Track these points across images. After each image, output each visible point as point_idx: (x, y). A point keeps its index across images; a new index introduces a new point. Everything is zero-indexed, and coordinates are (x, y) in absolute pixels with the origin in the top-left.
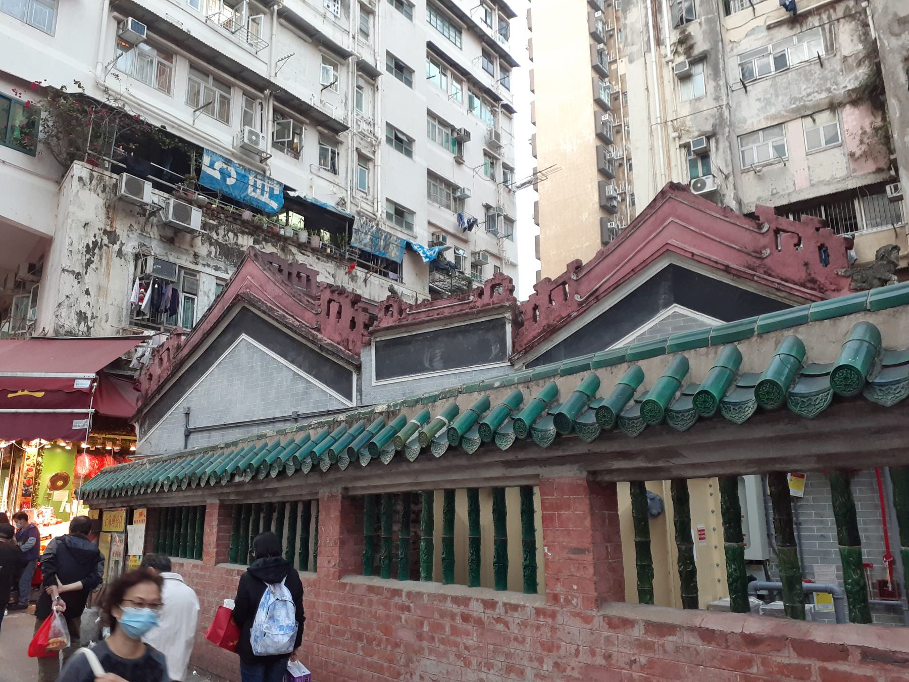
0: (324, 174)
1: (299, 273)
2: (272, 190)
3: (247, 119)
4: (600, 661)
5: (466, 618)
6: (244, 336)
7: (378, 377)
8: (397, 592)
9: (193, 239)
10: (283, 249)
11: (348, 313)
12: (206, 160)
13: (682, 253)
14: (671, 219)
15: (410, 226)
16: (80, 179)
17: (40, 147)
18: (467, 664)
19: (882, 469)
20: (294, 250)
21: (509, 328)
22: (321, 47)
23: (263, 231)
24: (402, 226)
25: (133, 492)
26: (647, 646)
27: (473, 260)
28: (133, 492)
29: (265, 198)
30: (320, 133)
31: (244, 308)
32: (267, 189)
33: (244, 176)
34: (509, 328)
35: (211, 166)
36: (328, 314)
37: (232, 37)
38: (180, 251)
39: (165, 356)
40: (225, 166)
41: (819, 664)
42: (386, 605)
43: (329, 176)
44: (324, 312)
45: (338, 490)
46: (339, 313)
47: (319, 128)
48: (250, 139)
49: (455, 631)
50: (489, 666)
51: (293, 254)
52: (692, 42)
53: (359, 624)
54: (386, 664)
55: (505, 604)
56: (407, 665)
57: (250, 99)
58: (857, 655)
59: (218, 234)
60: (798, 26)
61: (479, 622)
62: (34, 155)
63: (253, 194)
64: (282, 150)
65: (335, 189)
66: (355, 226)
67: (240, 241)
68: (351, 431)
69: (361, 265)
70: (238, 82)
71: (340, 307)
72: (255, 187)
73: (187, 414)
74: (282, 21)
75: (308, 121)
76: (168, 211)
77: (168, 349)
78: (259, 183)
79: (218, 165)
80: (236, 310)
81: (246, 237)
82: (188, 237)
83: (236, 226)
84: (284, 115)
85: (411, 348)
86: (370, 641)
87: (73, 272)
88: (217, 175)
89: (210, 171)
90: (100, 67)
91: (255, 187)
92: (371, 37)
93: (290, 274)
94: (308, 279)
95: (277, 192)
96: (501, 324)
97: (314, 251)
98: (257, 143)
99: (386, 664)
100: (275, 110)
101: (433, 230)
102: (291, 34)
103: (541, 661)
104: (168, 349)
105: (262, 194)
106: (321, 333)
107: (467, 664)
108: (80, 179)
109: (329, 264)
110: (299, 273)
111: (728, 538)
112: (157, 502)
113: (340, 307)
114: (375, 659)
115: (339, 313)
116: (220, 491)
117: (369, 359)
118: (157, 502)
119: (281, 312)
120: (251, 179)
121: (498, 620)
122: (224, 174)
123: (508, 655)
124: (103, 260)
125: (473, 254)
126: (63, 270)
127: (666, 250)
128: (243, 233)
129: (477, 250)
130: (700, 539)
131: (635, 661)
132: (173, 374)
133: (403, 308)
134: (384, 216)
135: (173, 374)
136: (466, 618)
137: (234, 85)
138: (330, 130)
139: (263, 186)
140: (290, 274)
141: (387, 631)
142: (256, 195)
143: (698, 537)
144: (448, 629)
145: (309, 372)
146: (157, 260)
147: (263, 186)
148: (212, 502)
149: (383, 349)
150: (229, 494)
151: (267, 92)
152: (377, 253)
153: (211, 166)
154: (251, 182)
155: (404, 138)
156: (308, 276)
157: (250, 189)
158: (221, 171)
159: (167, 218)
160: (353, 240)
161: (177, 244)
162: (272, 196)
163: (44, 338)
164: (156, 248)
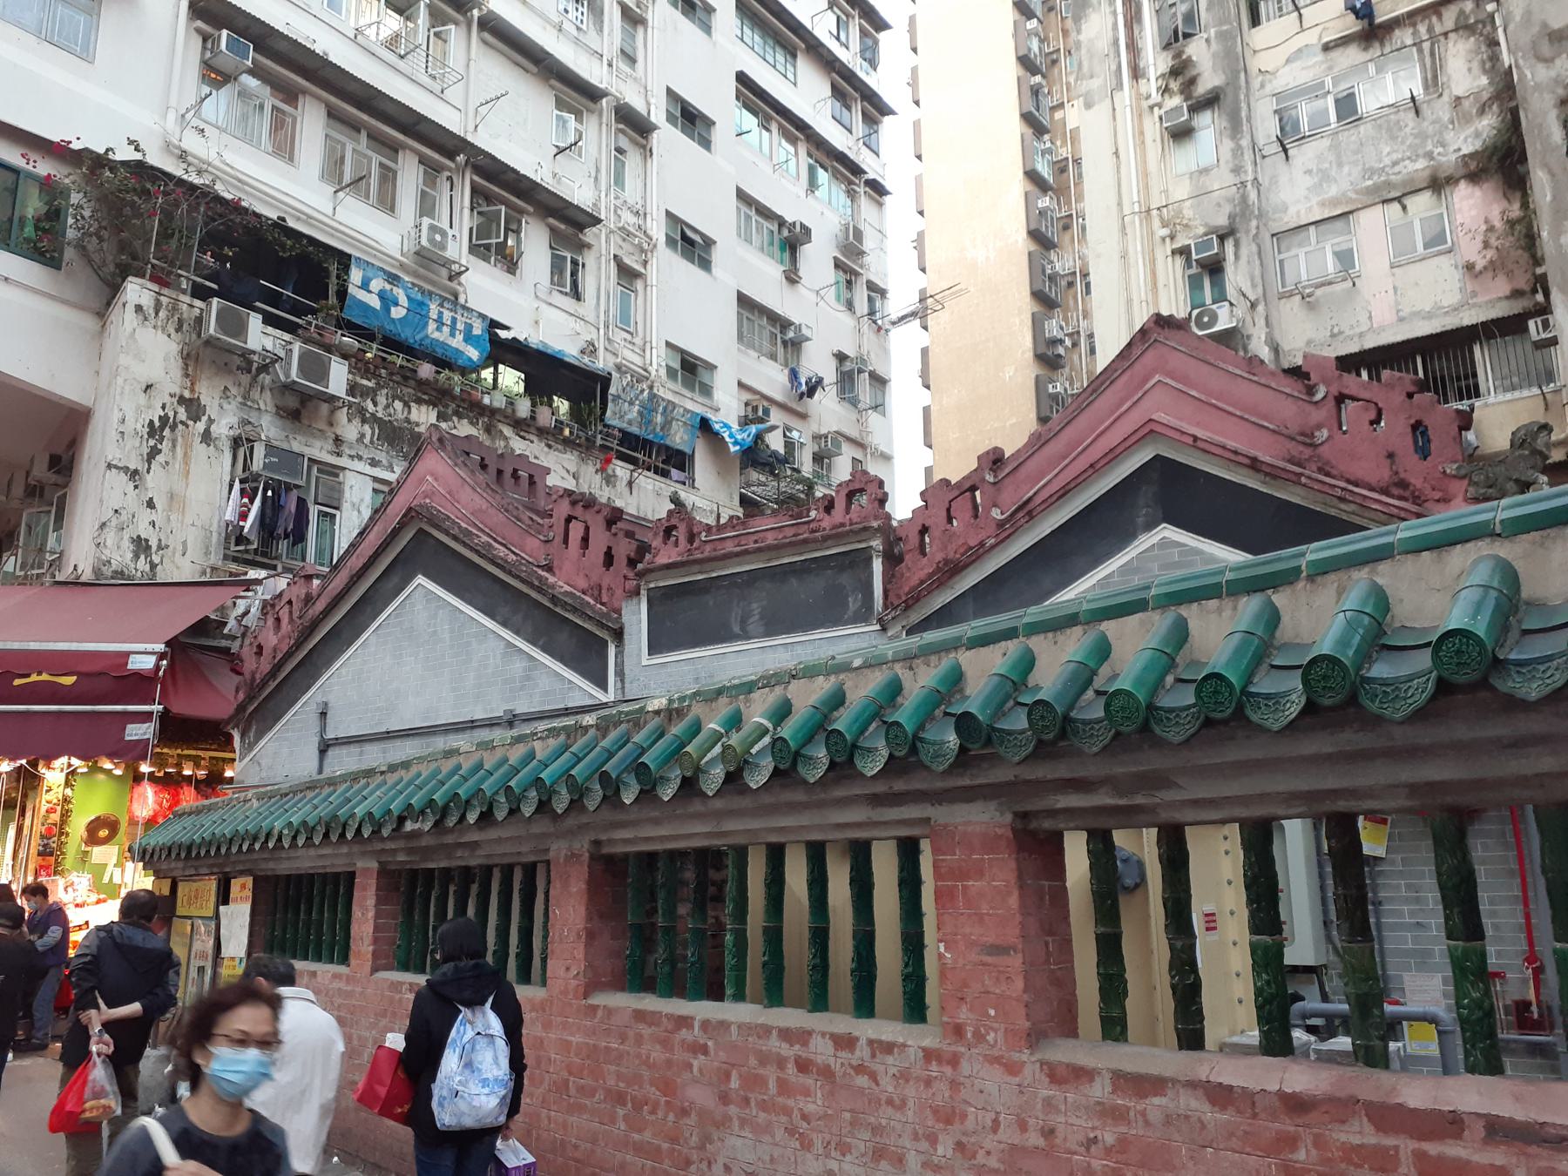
0: (559, 299)
1: (515, 471)
2: (469, 327)
3: (426, 206)
4: (1034, 1139)
5: (803, 1066)
6: (420, 580)
7: (653, 650)
8: (684, 1022)
9: (333, 412)
10: (488, 430)
11: (600, 540)
12: (356, 276)
13: (1177, 436)
14: (1157, 378)
15: (706, 391)
16: (139, 308)
17: (69, 253)
18: (806, 1145)
19: (1522, 808)
20: (507, 431)
21: (877, 566)
22: (553, 82)
23: (454, 398)
24: (693, 390)
25: (229, 849)
26: (1115, 1115)
27: (816, 448)
28: (229, 849)
29: (457, 342)
30: (553, 230)
31: (421, 531)
32: (460, 326)
33: (421, 304)
34: (877, 566)
35: (365, 286)
36: (566, 541)
37: (401, 64)
38: (311, 432)
39: (284, 614)
40: (388, 287)
41: (1413, 1145)
42: (665, 1043)
43: (568, 303)
44: (559, 539)
45: (582, 845)
46: (585, 540)
47: (551, 220)
48: (431, 240)
49: (784, 1087)
50: (844, 1149)
51: (506, 438)
52: (1194, 73)
53: (619, 1076)
54: (665, 1146)
55: (871, 1042)
56: (702, 1147)
57: (432, 171)
58: (1479, 1130)
59: (375, 404)
60: (1377, 45)
61: (827, 1073)
62: (59, 268)
63: (436, 335)
64: (486, 259)
65: (579, 326)
66: (612, 390)
67: (414, 416)
68: (605, 743)
69: (623, 457)
70: (410, 142)
71: (587, 529)
72: (440, 322)
73: (323, 714)
74: (486, 35)
75: (531, 209)
76: (290, 364)
77: (290, 602)
78: (447, 315)
79: (377, 284)
80: (408, 535)
81: (424, 408)
82: (325, 408)
83: (407, 390)
84: (489, 198)
85: (710, 600)
86: (638, 1105)
87: (126, 469)
88: (375, 302)
89: (361, 295)
90: (172, 116)
91: (440, 322)
92: (640, 64)
93: (500, 472)
94: (532, 481)
95: (477, 331)
96: (864, 558)
97: (542, 433)
98: (443, 247)
99: (665, 1146)
100: (475, 190)
101: (747, 396)
102: (502, 59)
103: (933, 1140)
104: (290, 602)
105: (452, 335)
106: (554, 574)
107: (806, 1145)
108: (139, 308)
109: (568, 455)
110: (515, 471)
111: (1255, 928)
112: (271, 865)
113: (587, 529)
114: (647, 1136)
115: (585, 540)
116: (379, 846)
117: (637, 618)
118: (271, 865)
119: (485, 538)
120: (434, 309)
121: (860, 1069)
122: (387, 300)
123: (876, 1130)
124: (178, 449)
125: (817, 437)
126: (109, 466)
127: (1149, 431)
128: (419, 401)
129: (824, 431)
130: (1208, 929)
131: (1095, 1140)
132: (298, 645)
133: (695, 530)
134: (663, 372)
135: (298, 645)
136: (803, 1066)
137: (404, 147)
138: (569, 224)
139: (454, 320)
140: (500, 472)
141: (668, 1087)
142: (442, 336)
143: (1203, 926)
144: (772, 1085)
145: (533, 642)
146: (270, 449)
147: (454, 320)
148: (366, 866)
149: (660, 602)
150: (394, 851)
151: (461, 158)
152: (650, 437)
153: (365, 286)
154: (434, 315)
155: (697, 238)
156: (531, 476)
157: (432, 326)
158: (382, 295)
159: (287, 375)
160: (609, 413)
161: (305, 421)
162: (469, 338)
163: (76, 584)
164: (270, 428)
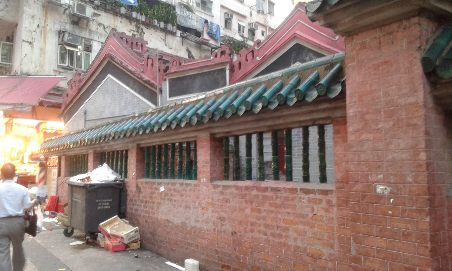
1: (137, 43)
4: (210, 200)
5: (175, 190)
6: (109, 75)
7: (171, 96)
8: (154, 183)
9: (88, 22)
11: (157, 64)
13: (301, 38)
14: (299, 20)
15: (210, 10)
18: (175, 206)
19: (289, 131)
21: (228, 72)
24: (205, 10)
26: (222, 193)
27: (249, 28)
31: (109, 61)
34: (228, 72)
36: (147, 65)
38: (81, 28)
39: (73, 85)
41: (262, 193)
42: (151, 188)
44: (146, 64)
45: (135, 145)
46: (152, 65)
49: (172, 195)
50: (181, 206)
51: (142, 29)
53: (143, 197)
54: (151, 210)
55: (186, 184)
56: (157, 210)
58: (269, 190)
61: (179, 192)
68: (138, 120)
71: (153, 61)
73: (85, 113)
76: (74, 8)
77: (75, 81)
80: (105, 62)
82: (85, 21)
85: (185, 83)
86: (146, 202)
87: (28, 42)
93: (132, 43)
94: (142, 45)
96: (224, 70)
99: (151, 210)
101: (225, 11)
103: (195, 202)
104: (75, 81)
106: (144, 74)
107: (175, 206)
110: (137, 43)
111: (247, 156)
112: (69, 153)
113: (153, 61)
114: (147, 209)
115: (152, 65)
116: (92, 147)
117: (166, 87)
118: (69, 153)
119: (126, 64)
121: (184, 190)
123: (186, 202)
124: (42, 35)
125: (249, 24)
126: (23, 41)
127: (295, 37)
129: (252, 22)
131: (219, 199)
132: (78, 93)
133: (181, 62)
134: (195, 5)
135: (78, 93)
136: (175, 190)
140: (132, 43)
141: (151, 198)
144: (169, 195)
145: (139, 93)
146: (70, 34)
148: (91, 152)
149: (173, 83)
150: (97, 147)
156: (142, 44)
159: (73, 10)
161: (80, 25)
163: (15, 75)
164: (68, 27)
